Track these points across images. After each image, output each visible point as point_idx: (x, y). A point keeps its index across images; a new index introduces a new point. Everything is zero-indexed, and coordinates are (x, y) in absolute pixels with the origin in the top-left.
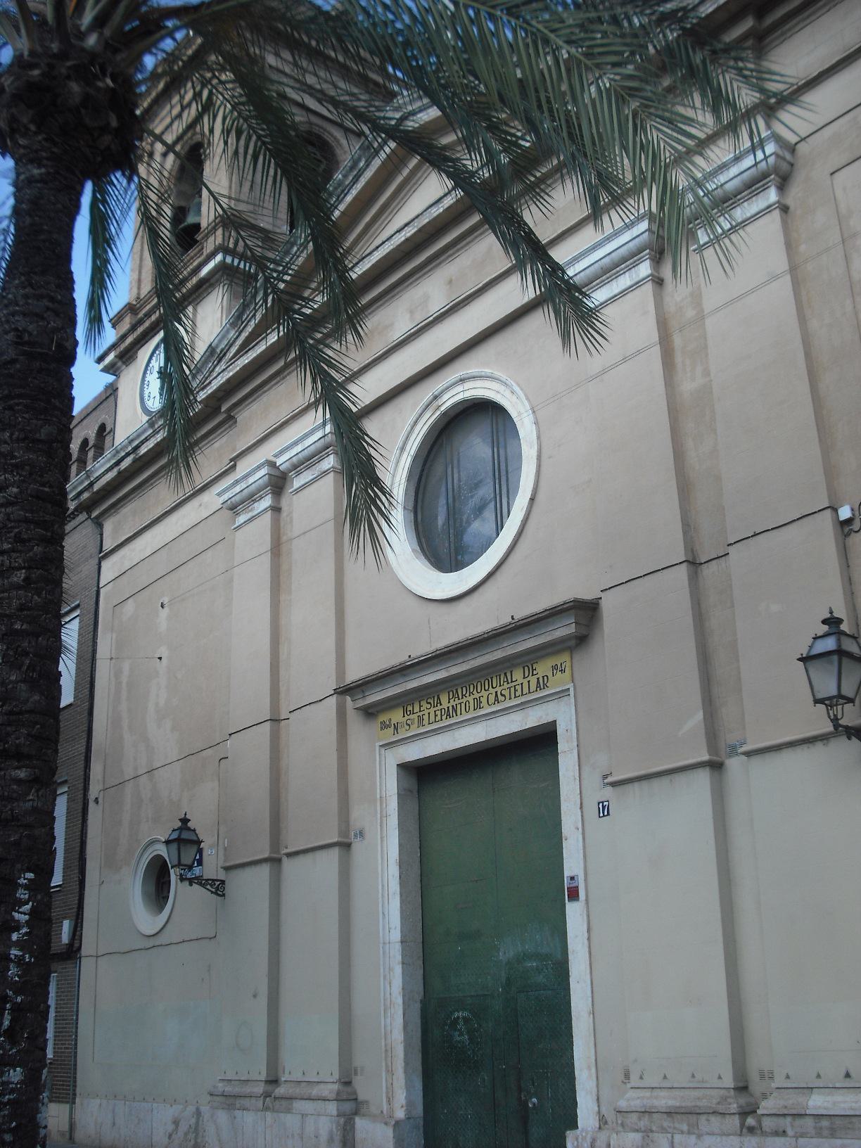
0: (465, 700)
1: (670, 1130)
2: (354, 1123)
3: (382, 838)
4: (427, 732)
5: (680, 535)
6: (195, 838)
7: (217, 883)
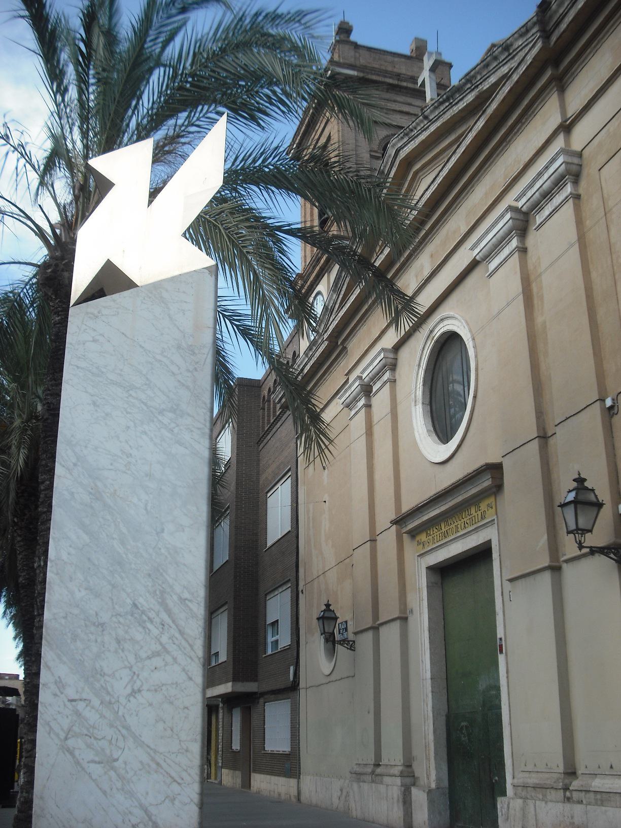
0: (451, 527)
1: (535, 798)
2: (411, 790)
3: (420, 614)
4: (437, 547)
5: (534, 420)
6: (334, 616)
7: (351, 643)
